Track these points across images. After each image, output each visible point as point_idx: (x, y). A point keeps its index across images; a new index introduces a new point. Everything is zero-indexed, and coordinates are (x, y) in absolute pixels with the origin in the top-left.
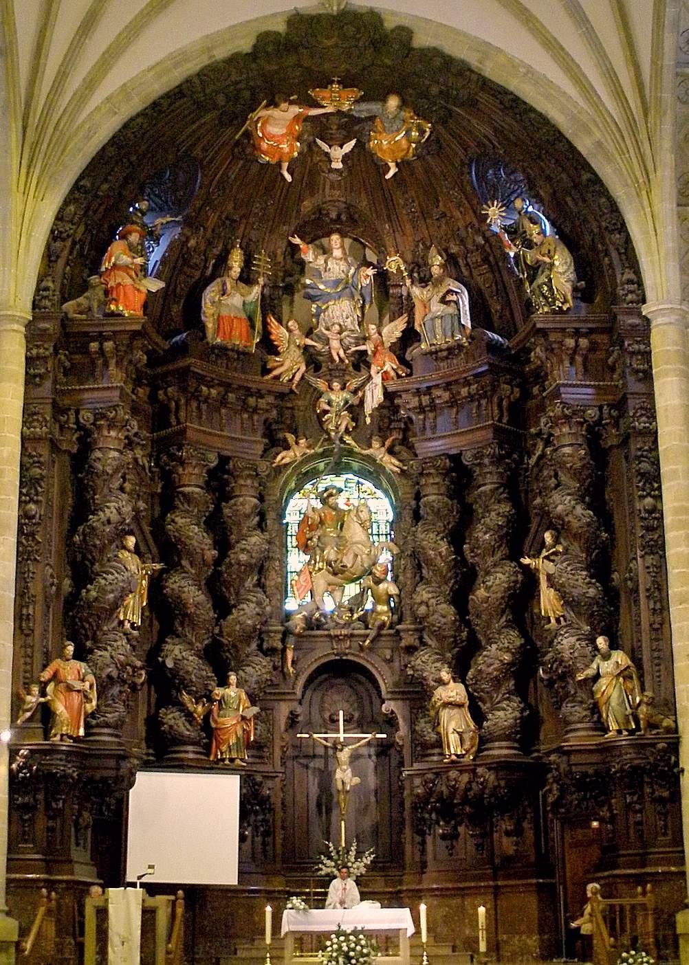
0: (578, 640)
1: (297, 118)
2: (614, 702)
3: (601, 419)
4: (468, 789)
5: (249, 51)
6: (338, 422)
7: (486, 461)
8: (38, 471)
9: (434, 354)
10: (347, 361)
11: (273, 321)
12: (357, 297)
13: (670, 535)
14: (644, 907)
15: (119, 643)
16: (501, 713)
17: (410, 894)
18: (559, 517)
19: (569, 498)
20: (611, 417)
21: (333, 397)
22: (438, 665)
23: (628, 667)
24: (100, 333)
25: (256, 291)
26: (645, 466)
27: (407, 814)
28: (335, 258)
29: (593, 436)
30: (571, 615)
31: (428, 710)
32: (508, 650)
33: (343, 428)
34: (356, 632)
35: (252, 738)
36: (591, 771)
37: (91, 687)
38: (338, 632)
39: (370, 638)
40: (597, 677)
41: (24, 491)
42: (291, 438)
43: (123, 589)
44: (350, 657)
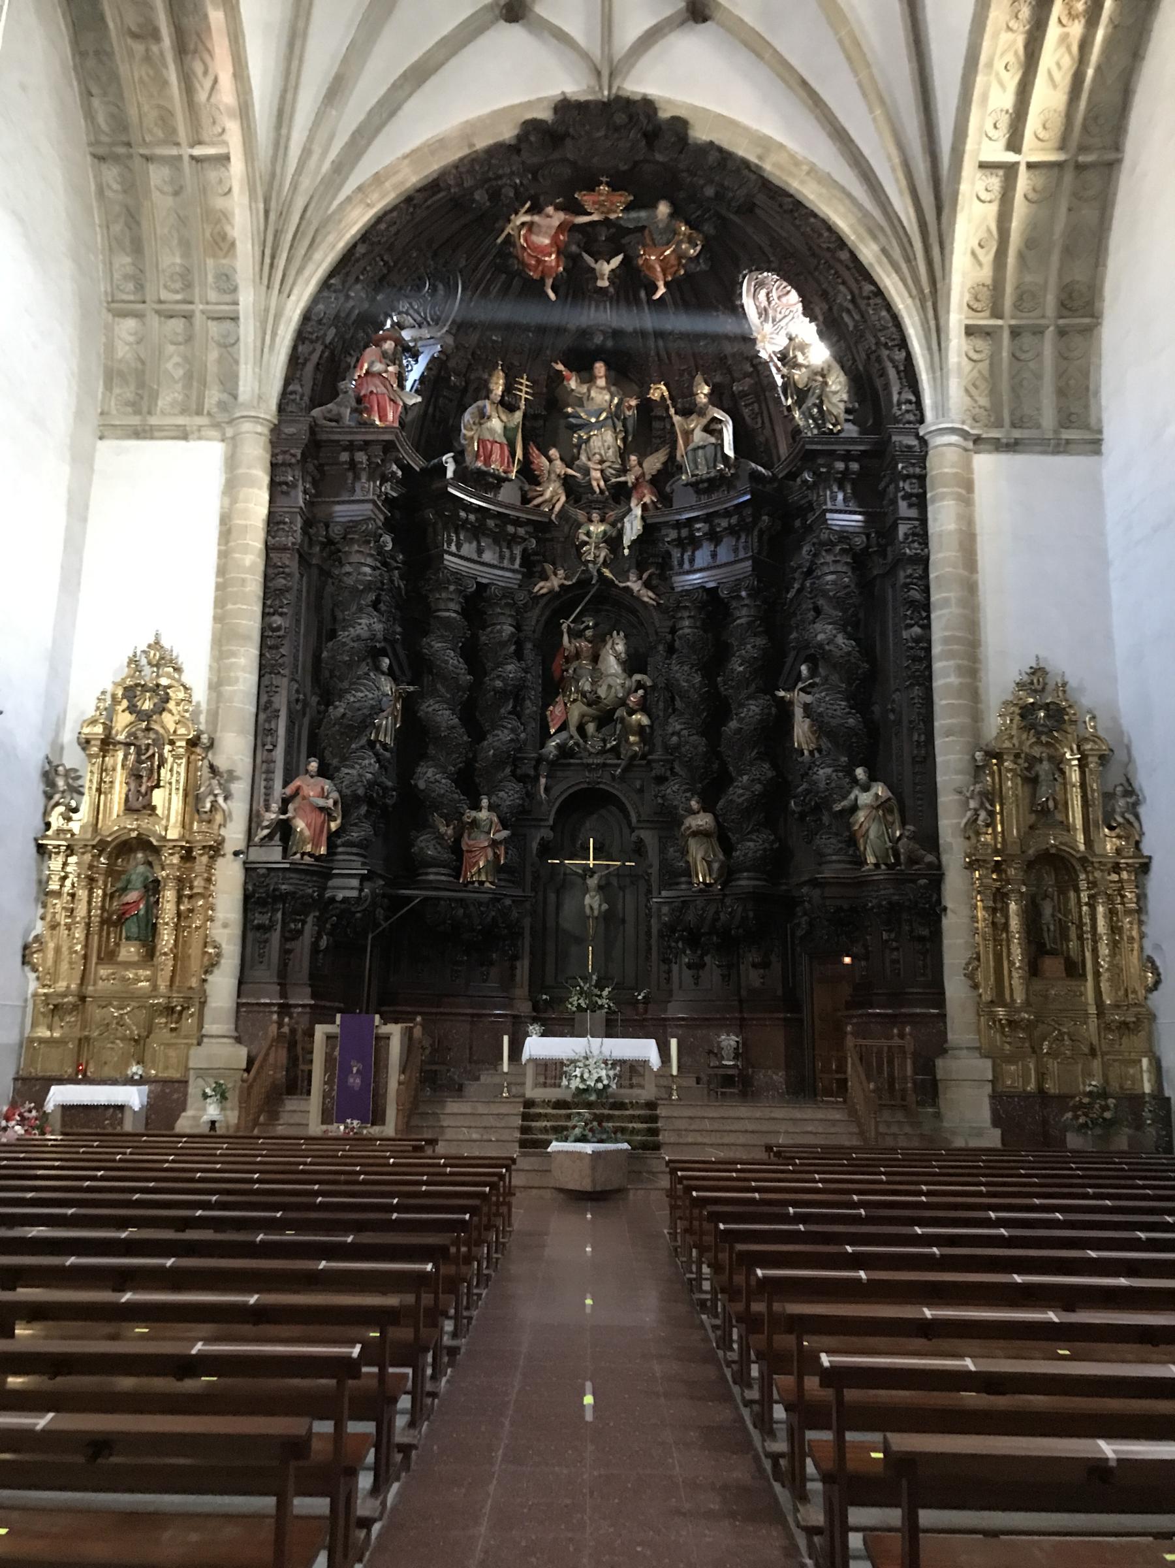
0: (836, 771)
2: (872, 834)
3: (868, 547)
4: (716, 919)
5: (513, 142)
6: (594, 553)
7: (743, 594)
8: (283, 581)
11: (534, 451)
12: (620, 427)
13: (938, 666)
14: (902, 1049)
15: (367, 762)
16: (751, 844)
18: (820, 646)
20: (878, 545)
21: (592, 528)
22: (688, 795)
23: (889, 799)
24: (351, 442)
26: (915, 595)
27: (654, 941)
29: (859, 560)
30: (825, 744)
32: (759, 781)
33: (601, 559)
37: (335, 803)
38: (590, 761)
40: (854, 808)
41: (269, 602)
42: (549, 567)
43: (372, 707)
44: (601, 786)
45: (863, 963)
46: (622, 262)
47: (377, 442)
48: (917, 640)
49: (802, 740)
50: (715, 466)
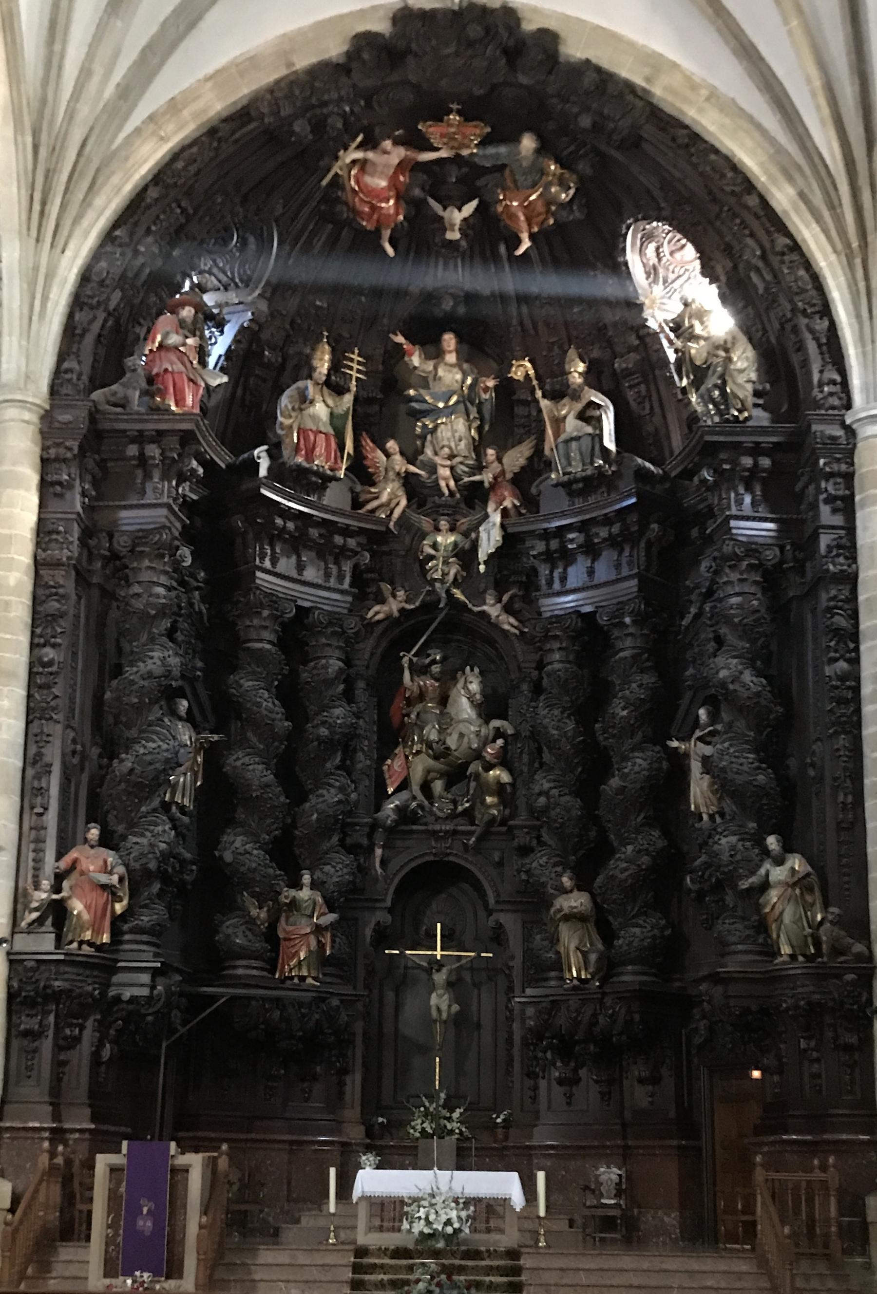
1: (401, 166)
2: (787, 918)
3: (782, 562)
4: (593, 1023)
5: (341, 61)
7: (627, 620)
8: (56, 605)
9: (568, 486)
10: (458, 496)
12: (474, 413)
14: (824, 1184)
15: (160, 828)
16: (637, 930)
17: (517, 1151)
18: (723, 684)
19: (735, 661)
20: (795, 559)
21: (439, 539)
22: (559, 869)
23: (808, 875)
24: (141, 432)
25: (348, 400)
26: (841, 621)
28: (446, 364)
31: (545, 924)
32: (647, 852)
33: (451, 578)
34: (460, 828)
35: (328, 953)
36: (754, 1008)
37: (121, 880)
38: (437, 827)
39: (476, 834)
42: (386, 587)
44: (451, 858)
45: (776, 1078)
46: (477, 209)
47: (173, 432)
48: (843, 678)
49: (700, 801)
50: (592, 462)
